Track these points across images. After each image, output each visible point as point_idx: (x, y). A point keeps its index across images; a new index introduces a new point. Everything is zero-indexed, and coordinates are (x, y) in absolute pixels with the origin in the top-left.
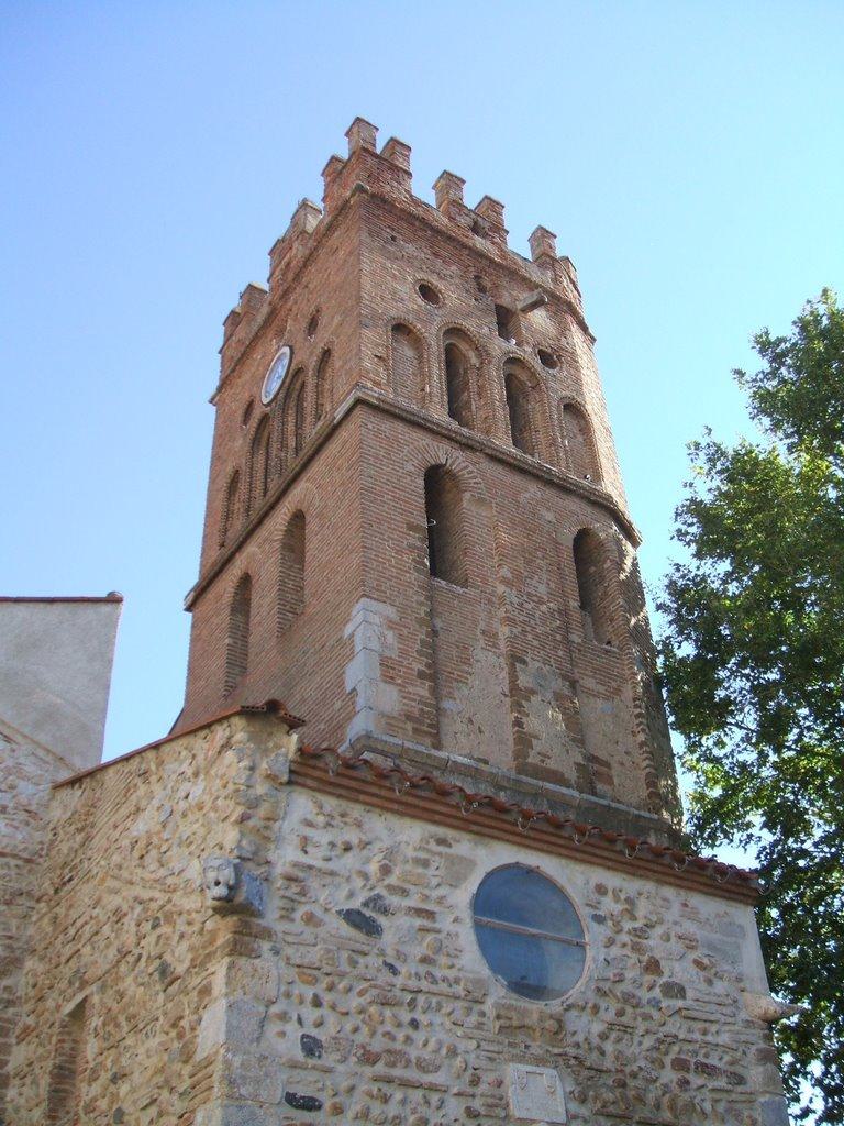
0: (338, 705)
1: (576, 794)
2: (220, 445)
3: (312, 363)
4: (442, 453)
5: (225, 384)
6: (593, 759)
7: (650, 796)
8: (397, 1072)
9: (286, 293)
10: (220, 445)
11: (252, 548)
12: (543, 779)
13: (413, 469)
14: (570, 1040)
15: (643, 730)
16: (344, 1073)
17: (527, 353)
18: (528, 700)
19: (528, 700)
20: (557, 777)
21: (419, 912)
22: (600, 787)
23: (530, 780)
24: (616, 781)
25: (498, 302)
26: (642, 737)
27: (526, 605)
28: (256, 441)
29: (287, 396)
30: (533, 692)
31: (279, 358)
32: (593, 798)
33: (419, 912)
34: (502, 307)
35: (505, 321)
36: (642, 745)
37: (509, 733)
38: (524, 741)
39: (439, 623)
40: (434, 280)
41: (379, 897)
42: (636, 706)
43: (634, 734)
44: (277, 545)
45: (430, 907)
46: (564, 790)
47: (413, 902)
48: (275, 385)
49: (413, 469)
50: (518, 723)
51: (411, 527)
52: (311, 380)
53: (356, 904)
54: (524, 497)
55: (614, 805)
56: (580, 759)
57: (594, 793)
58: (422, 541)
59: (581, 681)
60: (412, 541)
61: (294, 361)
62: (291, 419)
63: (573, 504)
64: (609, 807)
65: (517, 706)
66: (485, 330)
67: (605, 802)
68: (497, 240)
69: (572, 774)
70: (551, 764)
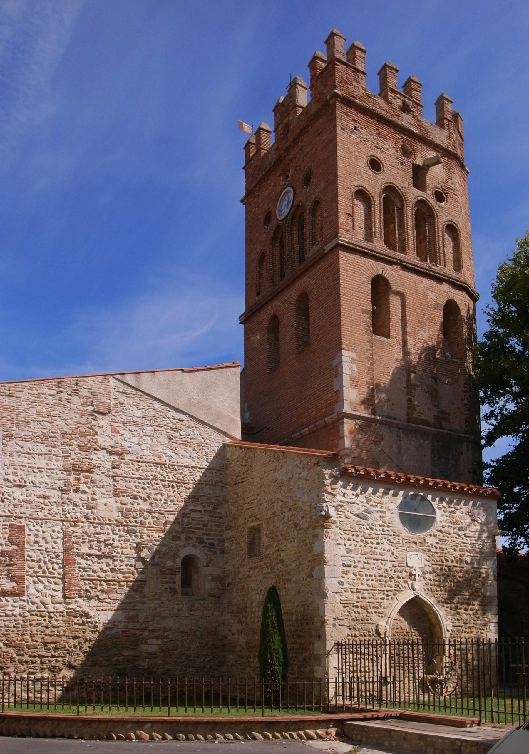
0: (330, 395)
1: (433, 429)
2: (251, 232)
3: (308, 206)
4: (380, 268)
5: (249, 193)
6: (443, 412)
7: (466, 426)
8: (374, 556)
9: (288, 150)
10: (251, 232)
11: (277, 302)
12: (419, 424)
13: (365, 280)
14: (426, 545)
15: (467, 398)
16: (357, 557)
17: (428, 196)
18: (415, 389)
19: (415, 389)
20: (426, 423)
21: (381, 512)
22: (444, 424)
23: (413, 425)
24: (451, 421)
25: (414, 162)
26: (465, 401)
27: (417, 345)
28: (274, 238)
29: (293, 218)
30: (417, 386)
31: (286, 192)
32: (440, 430)
33: (381, 512)
34: (416, 165)
35: (419, 175)
36: (465, 404)
37: (405, 405)
38: (411, 408)
39: (375, 357)
40: (379, 155)
41: (368, 508)
42: (465, 387)
43: (462, 399)
44: (293, 307)
45: (384, 510)
46: (428, 428)
47: (378, 509)
48: (286, 210)
49: (365, 280)
50: (409, 400)
51: (364, 312)
52: (308, 218)
53: (360, 511)
54: (420, 287)
55: (449, 432)
56: (436, 414)
57: (441, 428)
58: (369, 318)
59: (440, 378)
60: (365, 319)
61: (295, 201)
62: (295, 232)
63: (445, 287)
64: (447, 433)
65: (409, 393)
66: (406, 185)
67: (445, 431)
68: (416, 114)
69: (432, 420)
70: (423, 417)
